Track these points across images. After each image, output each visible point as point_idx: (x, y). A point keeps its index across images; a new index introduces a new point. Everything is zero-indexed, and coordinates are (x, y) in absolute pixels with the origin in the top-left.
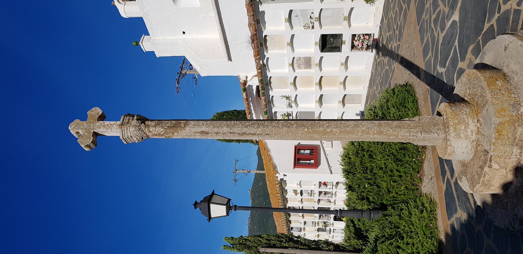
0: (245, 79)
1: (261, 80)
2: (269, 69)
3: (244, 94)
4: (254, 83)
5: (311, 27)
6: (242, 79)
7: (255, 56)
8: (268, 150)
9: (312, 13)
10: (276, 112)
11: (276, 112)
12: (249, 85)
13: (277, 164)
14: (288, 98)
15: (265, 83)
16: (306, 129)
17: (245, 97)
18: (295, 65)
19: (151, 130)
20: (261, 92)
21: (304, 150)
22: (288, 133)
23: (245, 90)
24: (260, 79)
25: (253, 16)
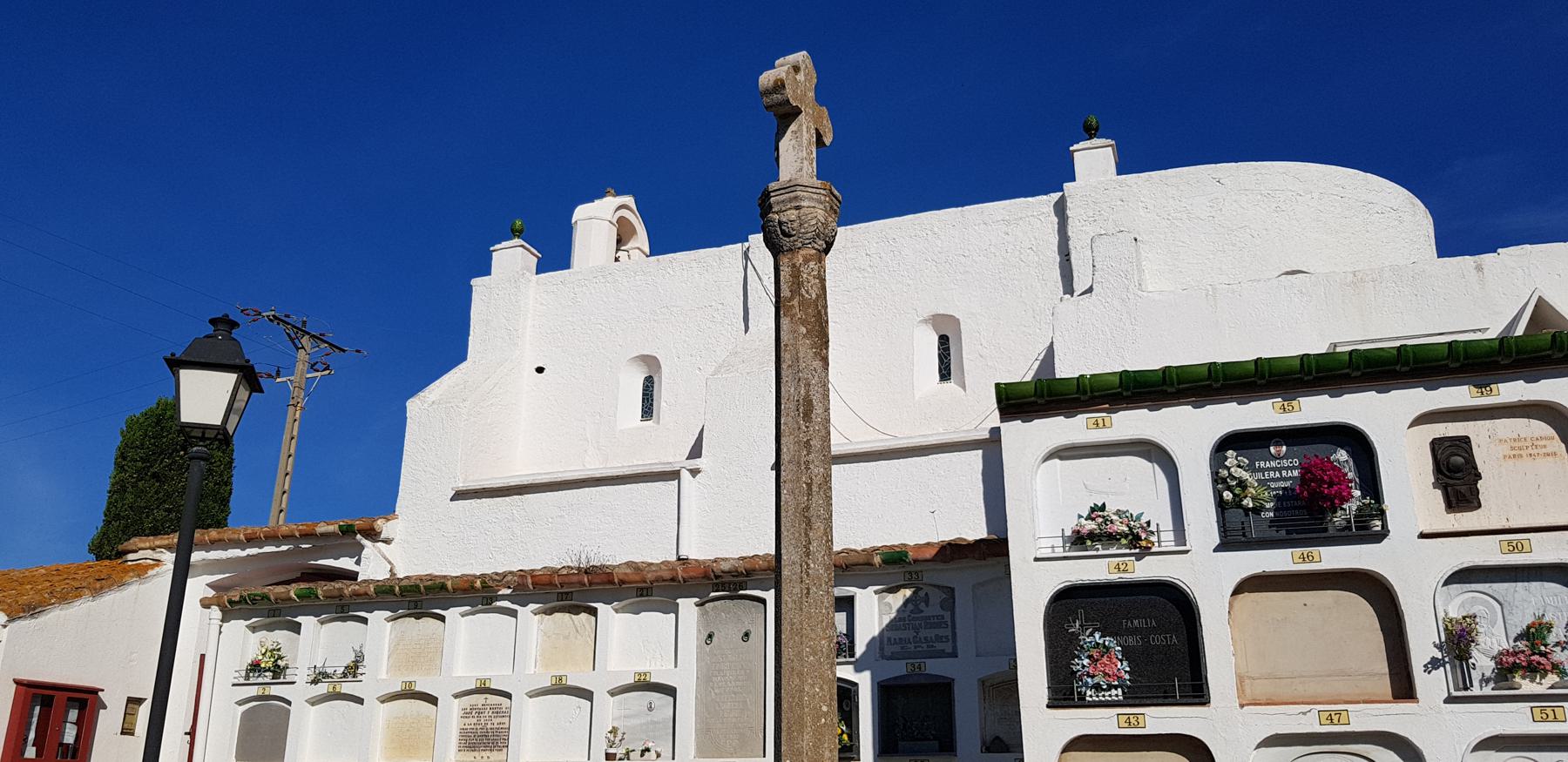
0: (383, 536)
1: (443, 587)
2: (473, 613)
3: (331, 528)
4: (373, 565)
5: (611, 751)
6: (386, 528)
7: (522, 574)
8: (97, 592)
9: (658, 756)
10: (296, 628)
11: (296, 628)
12: (362, 547)
13: (42, 619)
14: (352, 671)
15: (348, 602)
16: (825, 709)
17: (322, 528)
18: (479, 699)
19: (812, 264)
20: (322, 588)
21: (79, 723)
22: (814, 653)
23: (348, 531)
24: (449, 584)
25: (673, 580)
